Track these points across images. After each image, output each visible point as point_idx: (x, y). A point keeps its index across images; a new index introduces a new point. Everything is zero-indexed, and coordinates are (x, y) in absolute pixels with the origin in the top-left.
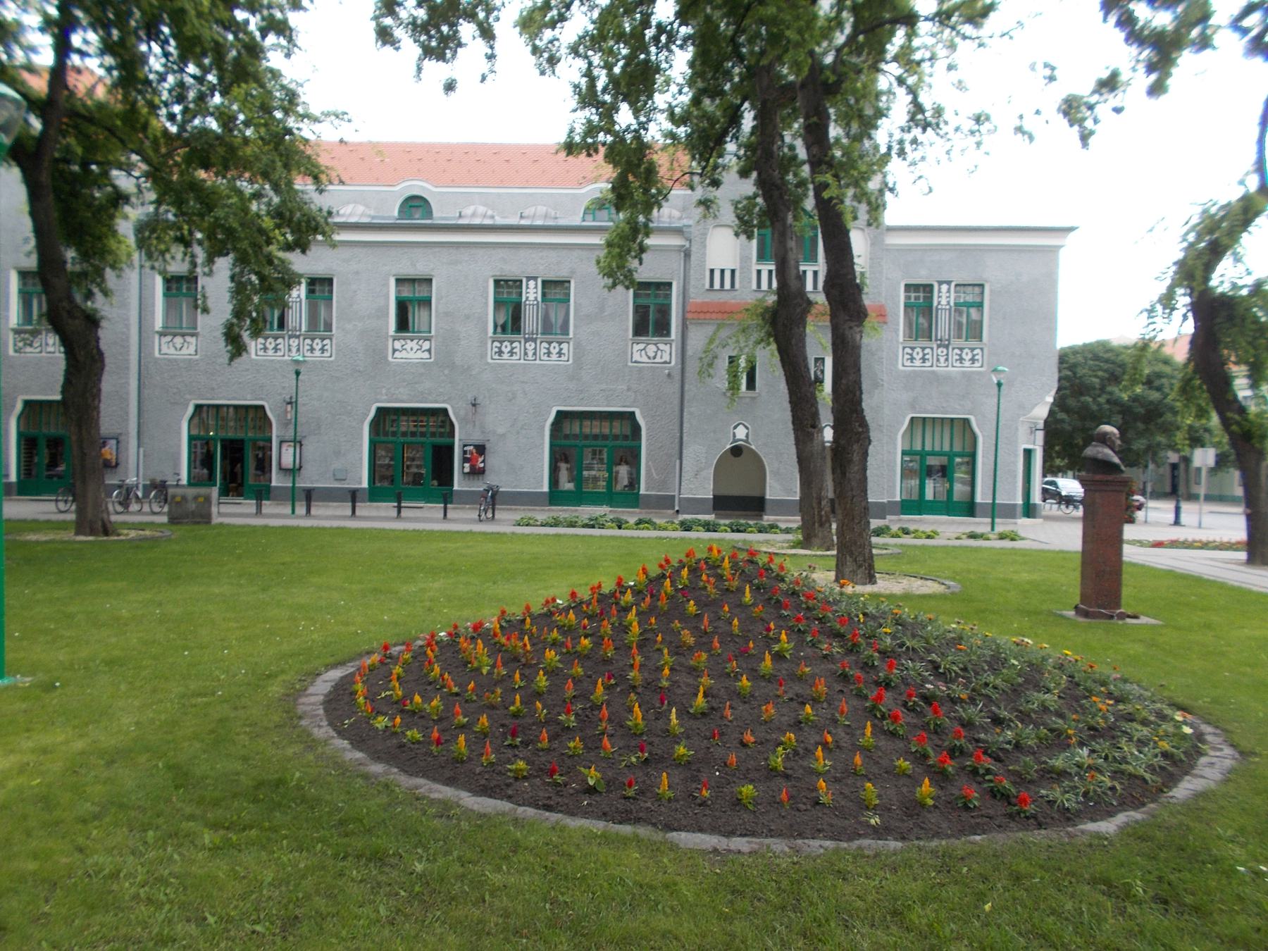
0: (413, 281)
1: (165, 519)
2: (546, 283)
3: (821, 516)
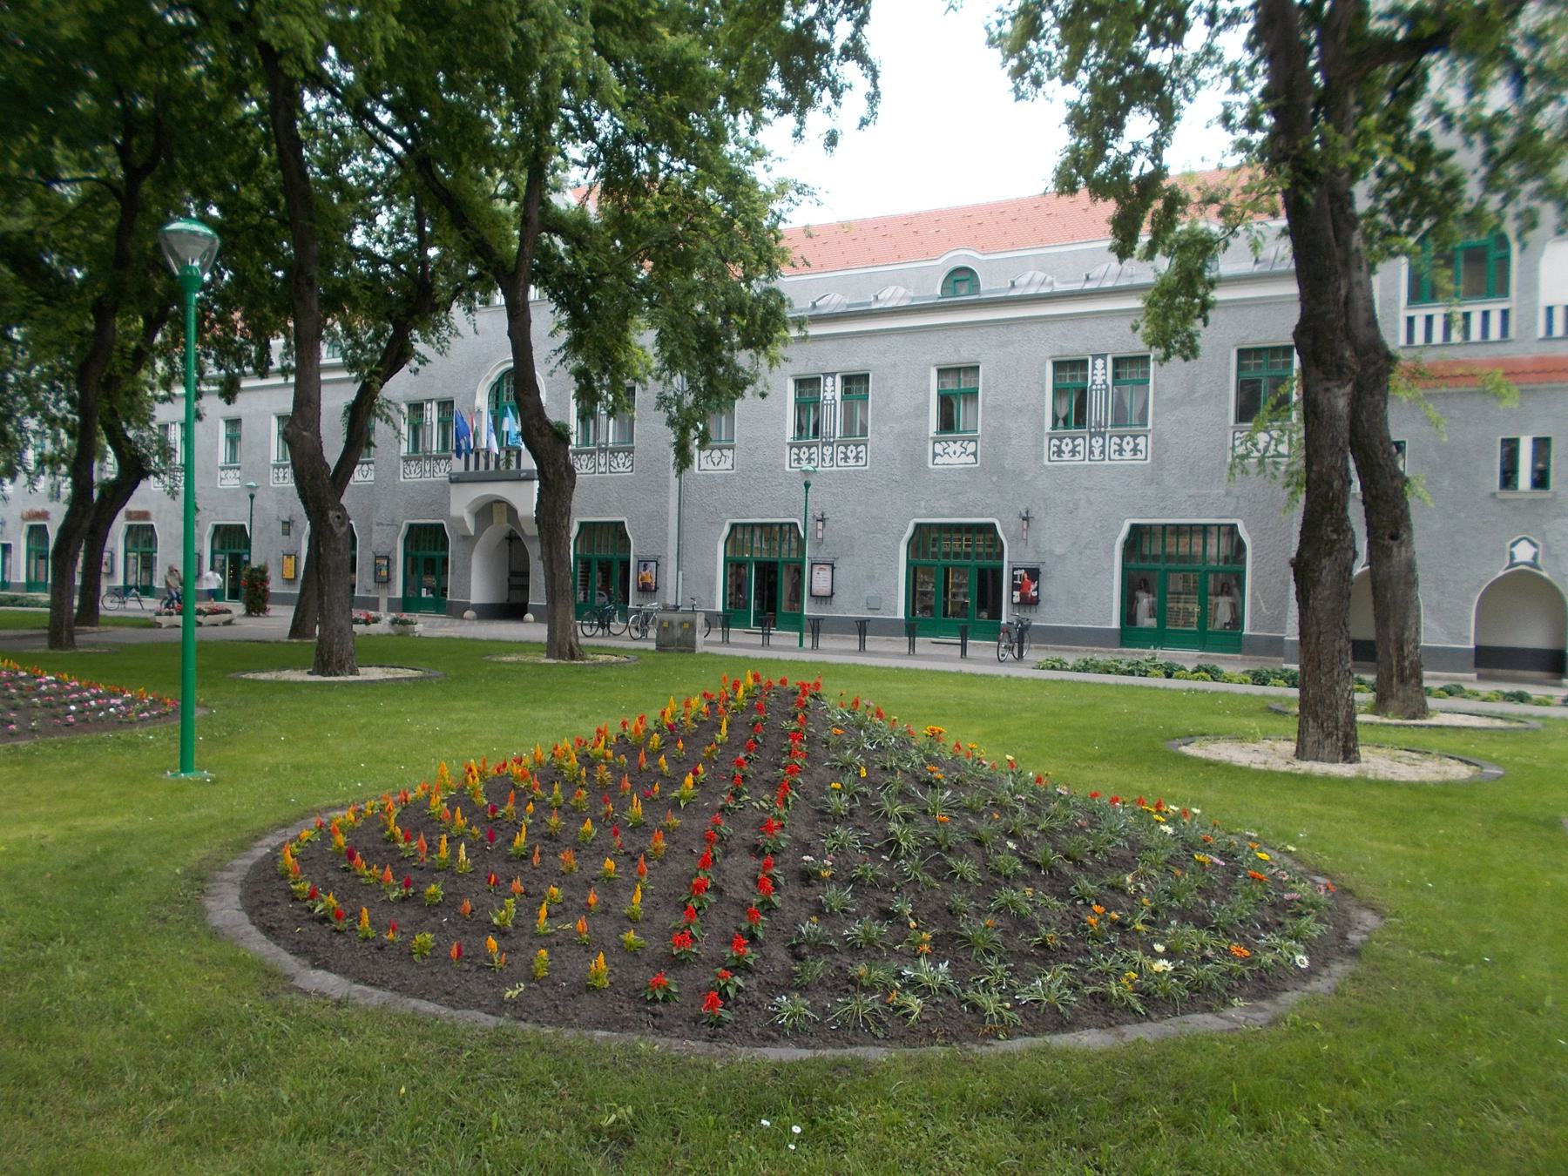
0: (957, 370)
1: (653, 646)
2: (1118, 362)
3: (1402, 669)
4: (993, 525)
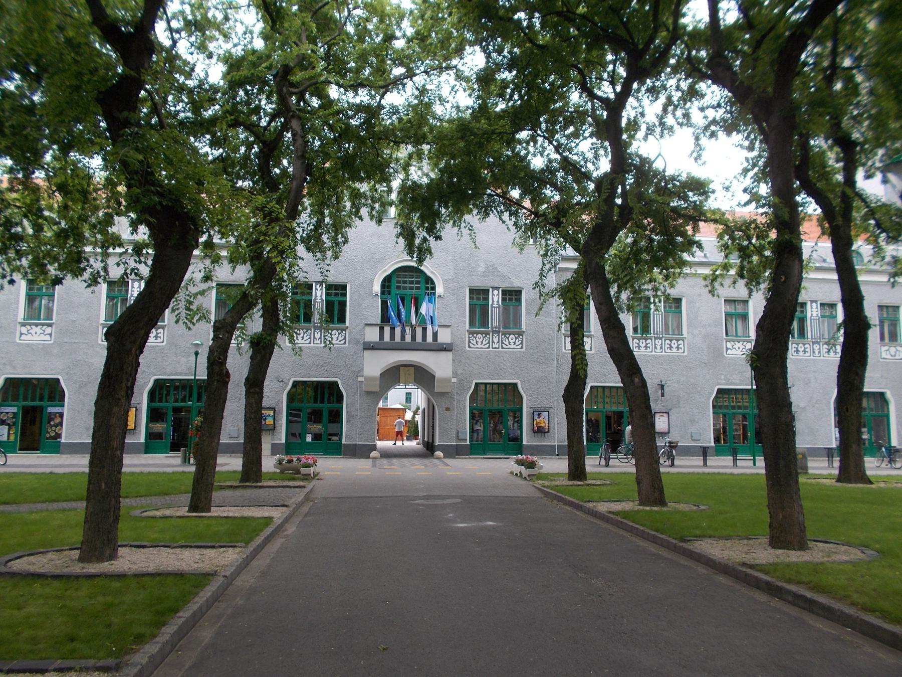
2: (504, 292)
4: (58, 380)
